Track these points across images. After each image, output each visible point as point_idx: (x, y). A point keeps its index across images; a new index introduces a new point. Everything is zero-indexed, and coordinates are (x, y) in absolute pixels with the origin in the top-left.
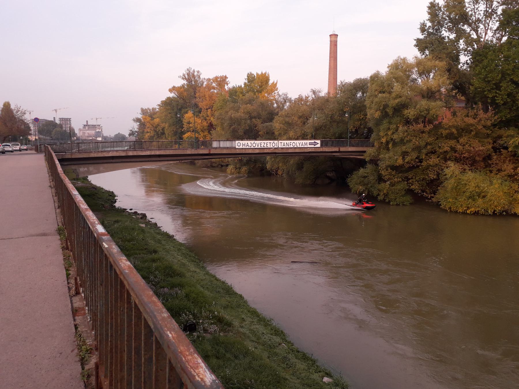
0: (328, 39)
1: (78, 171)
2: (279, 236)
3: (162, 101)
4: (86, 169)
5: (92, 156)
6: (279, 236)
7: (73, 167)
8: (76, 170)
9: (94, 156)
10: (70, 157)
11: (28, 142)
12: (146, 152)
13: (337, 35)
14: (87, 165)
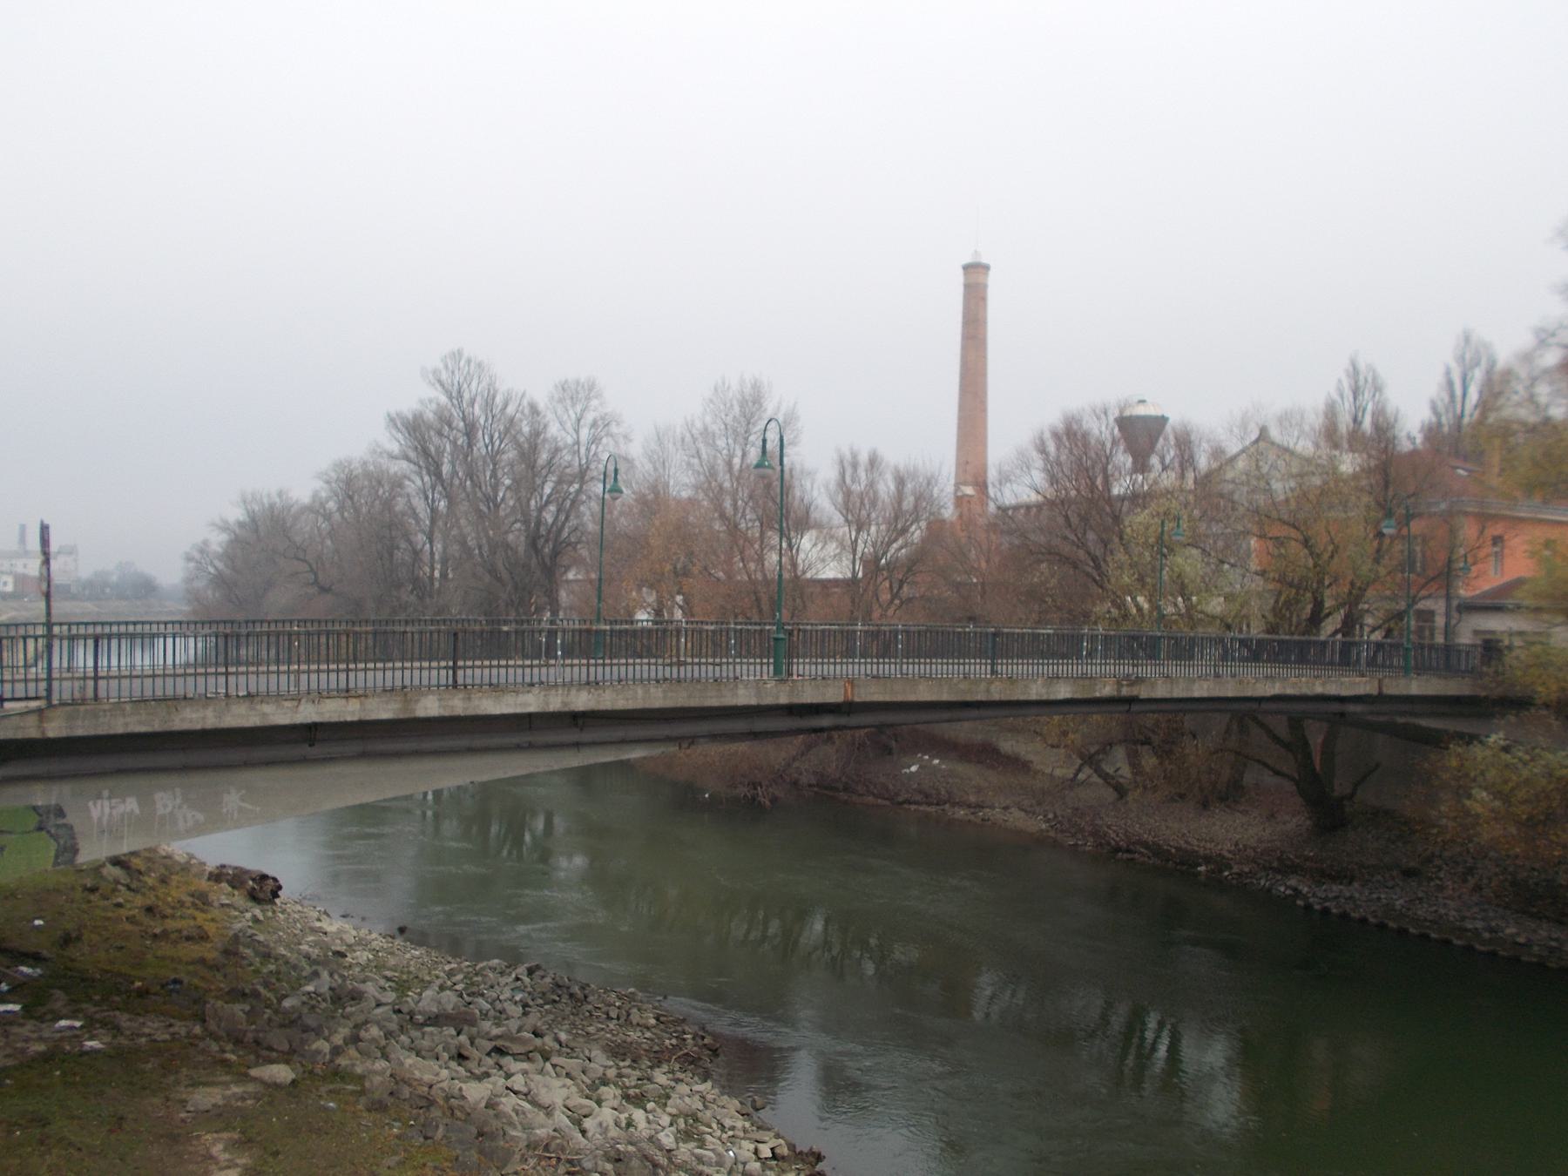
0: (958, 279)
1: (70, 819)
2: (34, 704)
3: (339, 466)
4: (132, 805)
5: (186, 726)
6: (34, 704)
7: (42, 796)
8: (60, 812)
9: (198, 727)
10: (33, 733)
11: (1539, 945)
12: (523, 698)
13: (986, 268)
14: (142, 782)
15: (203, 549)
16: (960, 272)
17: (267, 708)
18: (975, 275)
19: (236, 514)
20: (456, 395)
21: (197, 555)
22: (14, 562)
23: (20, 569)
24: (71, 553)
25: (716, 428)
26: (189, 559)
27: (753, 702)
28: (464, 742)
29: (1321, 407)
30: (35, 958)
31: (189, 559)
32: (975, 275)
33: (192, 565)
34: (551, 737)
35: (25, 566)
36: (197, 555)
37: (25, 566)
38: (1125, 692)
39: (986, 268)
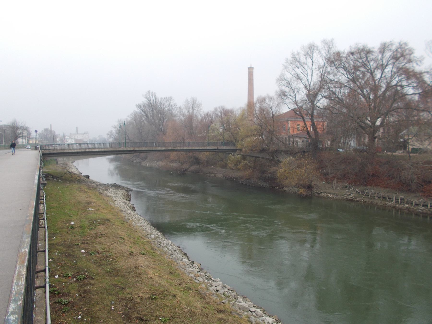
1: (57, 160)
4: (62, 159)
7: (55, 158)
8: (56, 159)
13: (253, 68)
15: (111, 132)
16: (247, 69)
17: (72, 150)
18: (251, 71)
19: (116, 124)
20: (149, 100)
21: (110, 134)
22: (75, 136)
23: (76, 138)
24: (87, 134)
25: (412, 56)
26: (108, 134)
27: (122, 150)
28: (92, 154)
29: (206, 113)
30: (58, 177)
31: (108, 134)
32: (251, 71)
33: (109, 136)
34: (101, 153)
35: (77, 137)
36: (110, 134)
37: (77, 137)
38: (173, 149)
39: (253, 68)
